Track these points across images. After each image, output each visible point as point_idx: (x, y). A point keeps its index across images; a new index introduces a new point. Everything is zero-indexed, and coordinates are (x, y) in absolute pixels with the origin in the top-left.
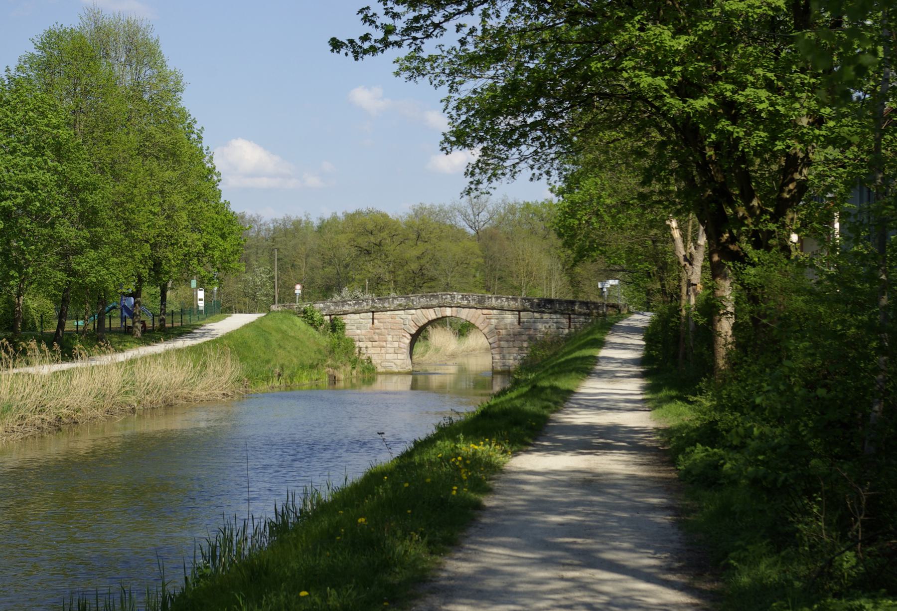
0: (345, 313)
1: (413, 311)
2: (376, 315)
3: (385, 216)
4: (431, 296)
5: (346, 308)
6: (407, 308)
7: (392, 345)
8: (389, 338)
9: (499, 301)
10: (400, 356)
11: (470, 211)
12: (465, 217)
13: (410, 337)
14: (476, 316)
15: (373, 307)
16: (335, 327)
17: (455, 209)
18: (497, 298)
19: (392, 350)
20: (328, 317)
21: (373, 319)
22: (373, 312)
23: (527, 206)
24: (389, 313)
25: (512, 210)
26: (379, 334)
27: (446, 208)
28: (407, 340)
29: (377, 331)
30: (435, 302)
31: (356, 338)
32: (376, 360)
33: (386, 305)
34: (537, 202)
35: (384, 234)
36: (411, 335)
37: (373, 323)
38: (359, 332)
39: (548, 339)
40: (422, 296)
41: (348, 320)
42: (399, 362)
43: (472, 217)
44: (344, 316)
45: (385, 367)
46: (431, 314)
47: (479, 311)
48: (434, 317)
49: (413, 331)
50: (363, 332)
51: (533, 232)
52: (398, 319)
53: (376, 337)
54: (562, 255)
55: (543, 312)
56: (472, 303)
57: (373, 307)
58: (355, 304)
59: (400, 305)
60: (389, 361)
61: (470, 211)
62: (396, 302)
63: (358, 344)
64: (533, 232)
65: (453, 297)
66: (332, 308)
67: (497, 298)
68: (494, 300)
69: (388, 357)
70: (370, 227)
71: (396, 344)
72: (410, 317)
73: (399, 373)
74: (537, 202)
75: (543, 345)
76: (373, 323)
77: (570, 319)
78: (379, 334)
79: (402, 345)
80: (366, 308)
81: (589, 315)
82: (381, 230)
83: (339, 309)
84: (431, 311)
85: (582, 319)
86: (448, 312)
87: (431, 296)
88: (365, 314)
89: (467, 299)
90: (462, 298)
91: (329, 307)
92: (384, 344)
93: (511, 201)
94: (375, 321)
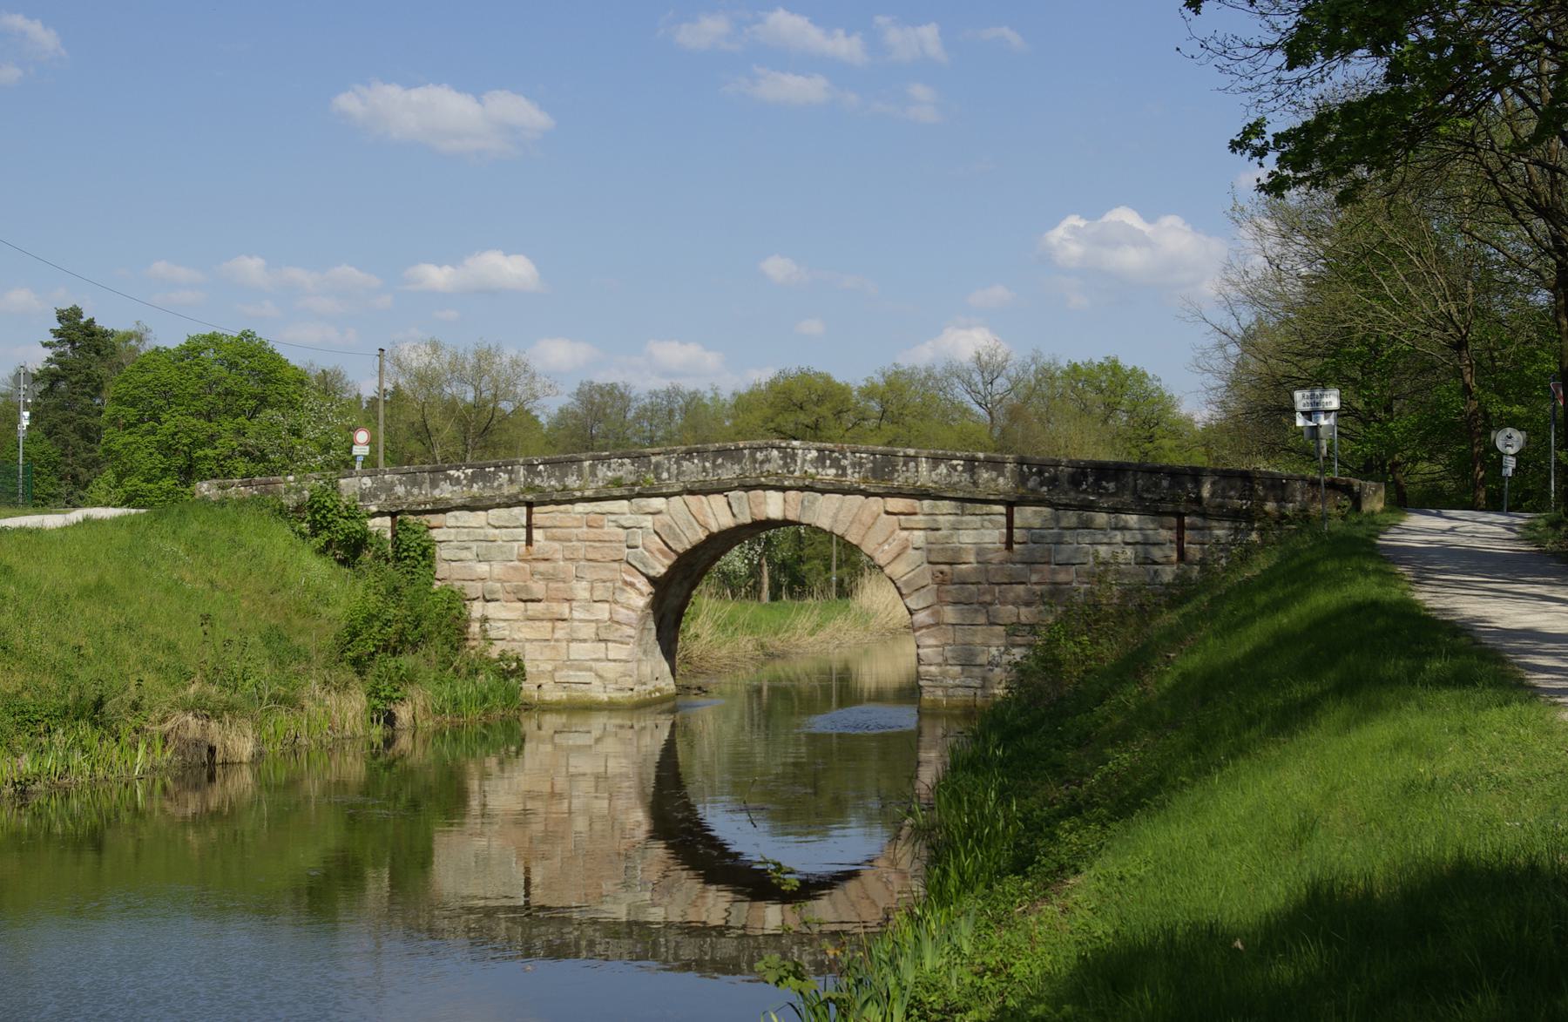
0: (442, 509)
1: (658, 503)
2: (540, 514)
3: (827, 379)
4: (720, 452)
5: (445, 491)
6: (634, 492)
7: (586, 615)
8: (581, 590)
9: (943, 469)
10: (615, 651)
11: (977, 378)
12: (971, 389)
13: (646, 588)
14: (866, 518)
15: (530, 488)
16: (413, 554)
17: (952, 374)
18: (936, 460)
19: (588, 631)
20: (387, 521)
21: (529, 527)
22: (530, 505)
23: (1075, 368)
24: (580, 507)
25: (1047, 375)
26: (548, 578)
27: (938, 371)
28: (639, 598)
29: (542, 566)
30: (729, 472)
31: (473, 589)
32: (537, 661)
33: (572, 481)
34: (1091, 362)
35: (825, 410)
36: (652, 581)
37: (529, 541)
38: (483, 568)
39: (1111, 595)
40: (689, 454)
41: (449, 531)
42: (610, 670)
43: (980, 386)
44: (434, 519)
45: (565, 685)
46: (718, 514)
47: (876, 504)
48: (727, 521)
49: (659, 568)
50: (498, 568)
51: (1085, 410)
52: (610, 530)
53: (538, 588)
54: (1134, 451)
55: (1090, 507)
56: (852, 477)
57: (530, 488)
58: (472, 480)
59: (617, 482)
60: (578, 666)
61: (977, 378)
62: (605, 473)
63: (477, 609)
64: (1085, 410)
65: (789, 457)
66: (400, 490)
67: (936, 460)
68: (924, 466)
69: (579, 651)
70: (798, 396)
71: (602, 612)
72: (648, 522)
73: (611, 707)
74: (1091, 362)
75: (1091, 617)
76: (529, 541)
77: (1181, 528)
78: (548, 578)
79: (622, 614)
80: (508, 490)
81: (1248, 516)
82: (820, 401)
83: (423, 494)
84: (718, 501)
85: (1221, 531)
86: (773, 505)
87: (720, 452)
88: (503, 512)
89: (836, 463)
90: (820, 461)
91: (390, 488)
92: (564, 609)
93: (1047, 358)
94: (537, 534)
